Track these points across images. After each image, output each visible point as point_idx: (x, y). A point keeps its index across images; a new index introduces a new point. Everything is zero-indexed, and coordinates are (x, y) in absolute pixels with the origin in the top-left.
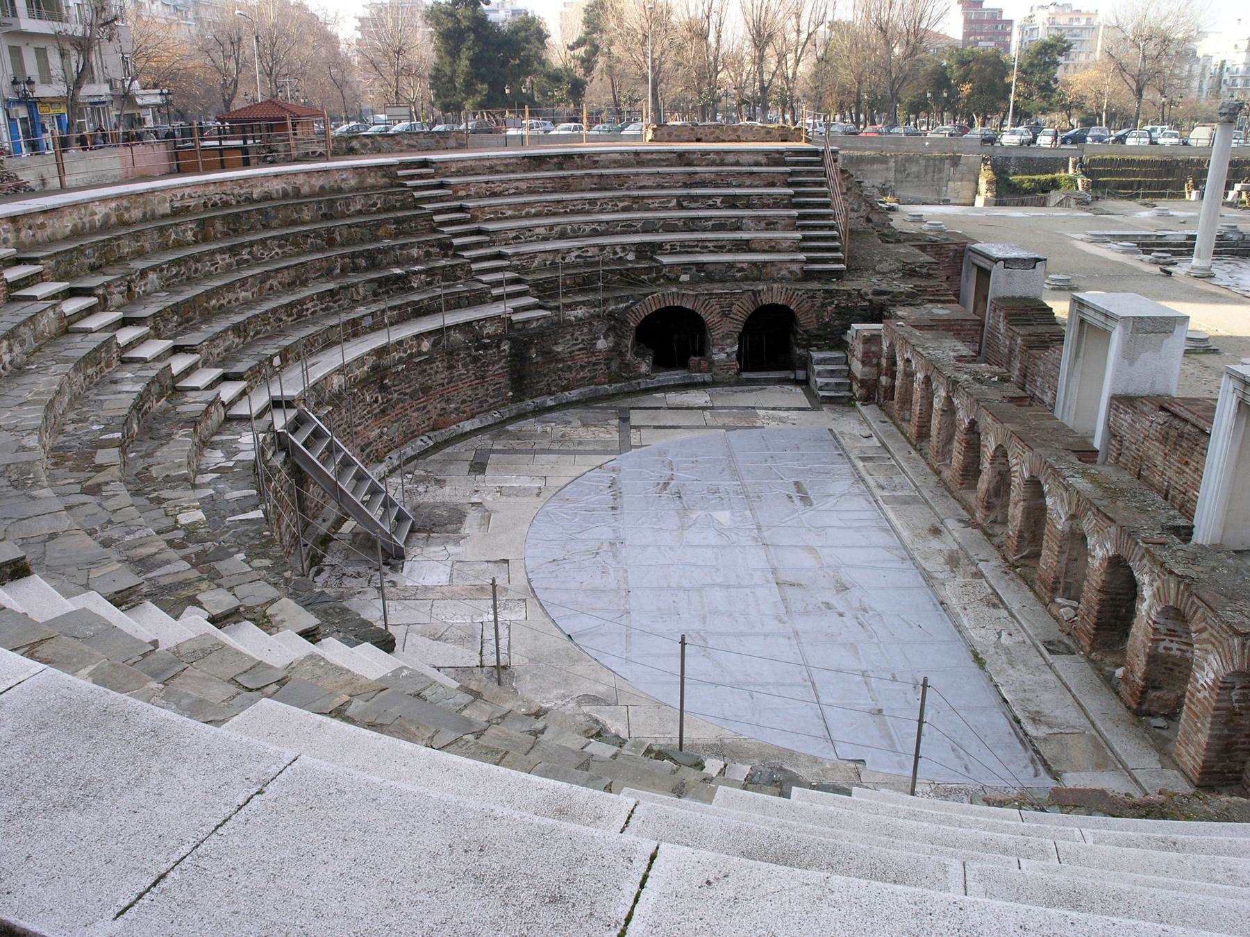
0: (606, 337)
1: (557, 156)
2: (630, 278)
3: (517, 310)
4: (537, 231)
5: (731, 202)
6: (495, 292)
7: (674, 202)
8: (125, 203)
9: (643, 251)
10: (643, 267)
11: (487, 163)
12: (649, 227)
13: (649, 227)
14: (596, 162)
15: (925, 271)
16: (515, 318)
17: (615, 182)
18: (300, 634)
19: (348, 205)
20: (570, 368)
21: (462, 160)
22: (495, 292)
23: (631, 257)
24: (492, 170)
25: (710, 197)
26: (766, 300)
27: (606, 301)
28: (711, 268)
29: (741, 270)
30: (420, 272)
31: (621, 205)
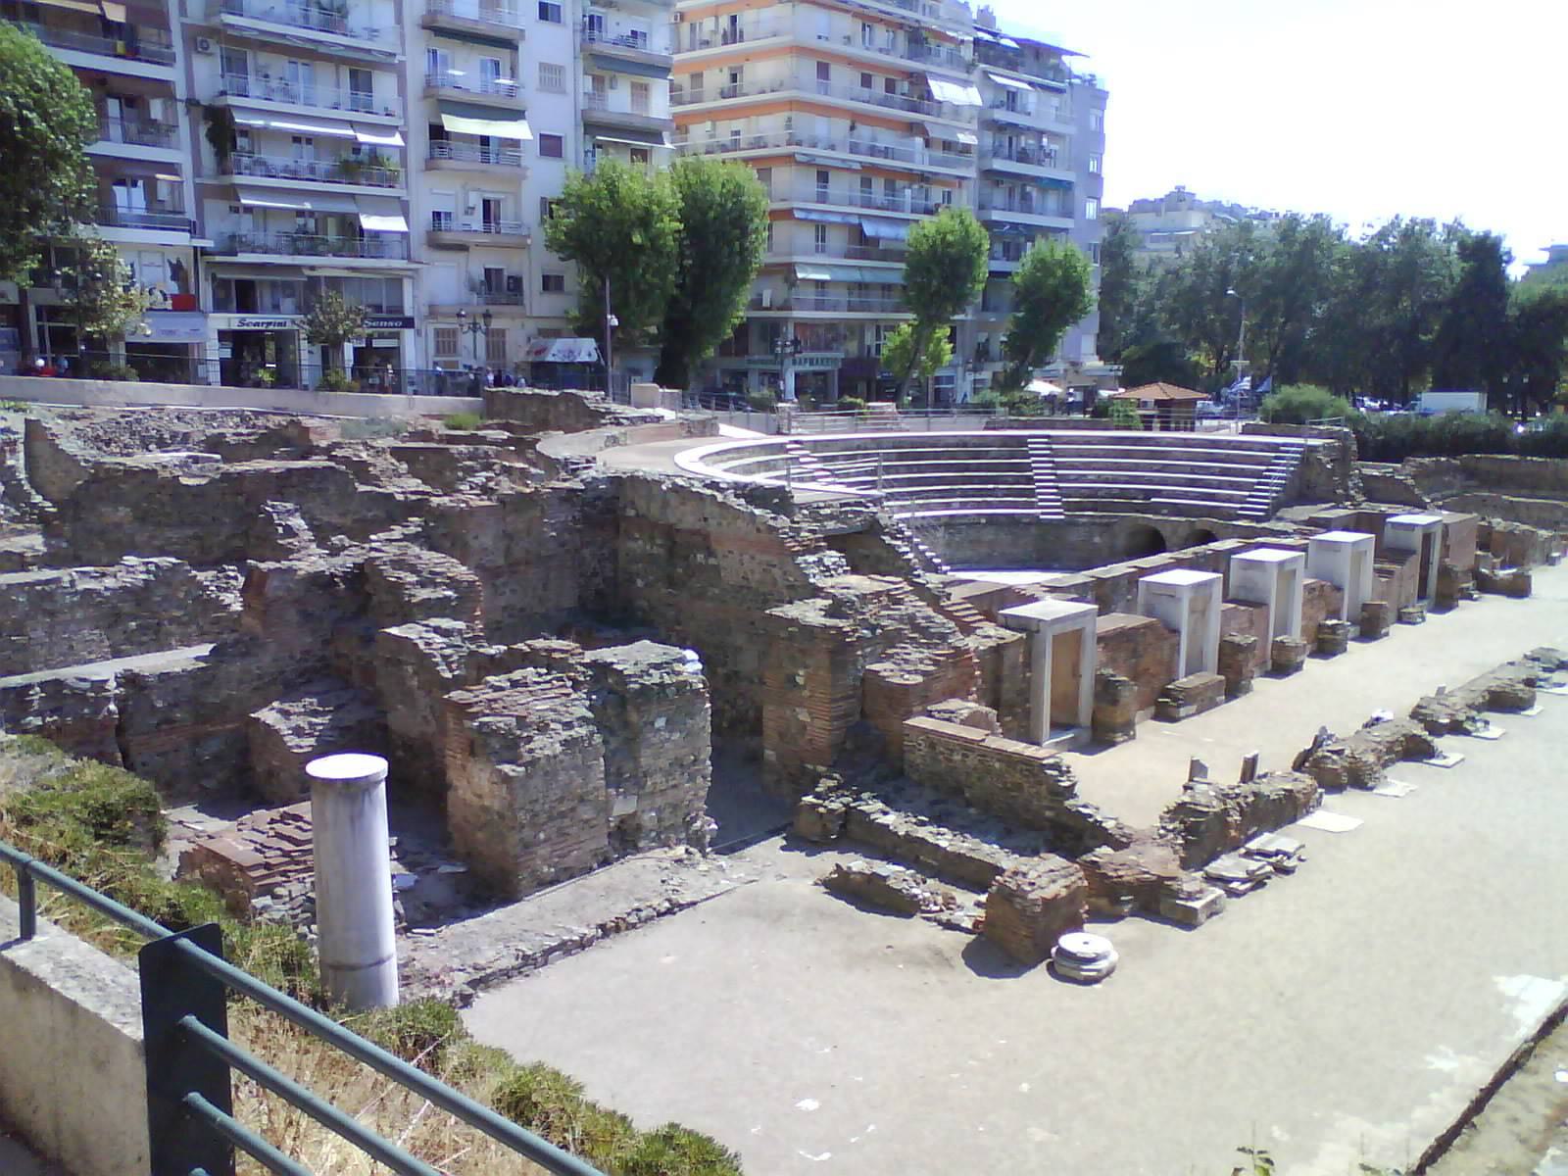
12: (1150, 481)
13: (1150, 481)
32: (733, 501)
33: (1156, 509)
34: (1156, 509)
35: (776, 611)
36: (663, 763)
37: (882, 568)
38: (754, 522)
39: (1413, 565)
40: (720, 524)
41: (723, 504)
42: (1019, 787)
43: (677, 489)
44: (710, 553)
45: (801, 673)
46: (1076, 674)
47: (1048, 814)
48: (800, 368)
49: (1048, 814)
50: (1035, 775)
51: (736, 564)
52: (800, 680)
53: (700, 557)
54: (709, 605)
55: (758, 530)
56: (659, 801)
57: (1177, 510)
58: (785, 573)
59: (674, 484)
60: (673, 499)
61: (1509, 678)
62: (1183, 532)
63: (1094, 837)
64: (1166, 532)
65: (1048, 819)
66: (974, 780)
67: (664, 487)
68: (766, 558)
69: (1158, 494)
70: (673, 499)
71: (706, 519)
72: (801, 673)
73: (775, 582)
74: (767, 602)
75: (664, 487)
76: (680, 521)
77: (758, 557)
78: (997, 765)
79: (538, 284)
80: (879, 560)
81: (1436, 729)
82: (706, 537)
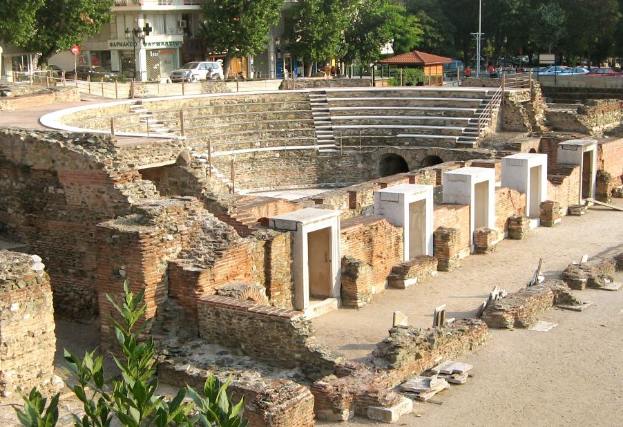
0: (362, 163)
1: (384, 91)
2: (383, 141)
3: (320, 148)
4: (354, 121)
5: (447, 114)
6: (319, 141)
7: (423, 113)
8: (192, 100)
9: (395, 131)
10: (392, 138)
11: (351, 93)
12: (396, 122)
13: (396, 122)
14: (401, 94)
15: (515, 147)
16: (320, 151)
17: (403, 103)
18: (425, 200)
19: (280, 106)
20: (345, 174)
21: (340, 92)
22: (319, 141)
23: (390, 133)
24: (353, 96)
25: (439, 111)
26: (429, 153)
27: (363, 149)
28: (418, 140)
29: (431, 141)
30: (292, 131)
31: (399, 113)
32: (71, 146)
33: (400, 142)
34: (400, 142)
35: (103, 224)
36: (20, 335)
37: (187, 190)
38: (87, 161)
39: (576, 174)
40: (63, 164)
41: (65, 150)
42: (277, 339)
43: (31, 140)
44: (59, 186)
45: (123, 267)
46: (328, 260)
47: (297, 356)
48: (148, 47)
49: (297, 356)
50: (286, 330)
51: (77, 194)
52: (123, 273)
53: (51, 188)
54: (60, 223)
55: (91, 167)
56: (18, 363)
57: (414, 142)
58: (111, 197)
59: (29, 136)
60: (31, 149)
61: (294, 256)
62: (420, 157)
63: (326, 369)
64: (408, 159)
65: (298, 360)
66: (246, 336)
67: (22, 138)
68: (97, 186)
69: (402, 130)
70: (31, 149)
71: (53, 161)
72: (123, 267)
73: (105, 205)
74: (99, 219)
75: (22, 138)
76: (35, 163)
77: (92, 186)
78: (261, 324)
79: (564, 211)
80: (184, 185)
81: (575, 285)
82: (55, 174)
